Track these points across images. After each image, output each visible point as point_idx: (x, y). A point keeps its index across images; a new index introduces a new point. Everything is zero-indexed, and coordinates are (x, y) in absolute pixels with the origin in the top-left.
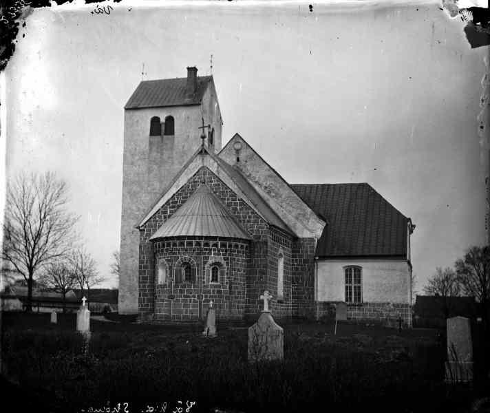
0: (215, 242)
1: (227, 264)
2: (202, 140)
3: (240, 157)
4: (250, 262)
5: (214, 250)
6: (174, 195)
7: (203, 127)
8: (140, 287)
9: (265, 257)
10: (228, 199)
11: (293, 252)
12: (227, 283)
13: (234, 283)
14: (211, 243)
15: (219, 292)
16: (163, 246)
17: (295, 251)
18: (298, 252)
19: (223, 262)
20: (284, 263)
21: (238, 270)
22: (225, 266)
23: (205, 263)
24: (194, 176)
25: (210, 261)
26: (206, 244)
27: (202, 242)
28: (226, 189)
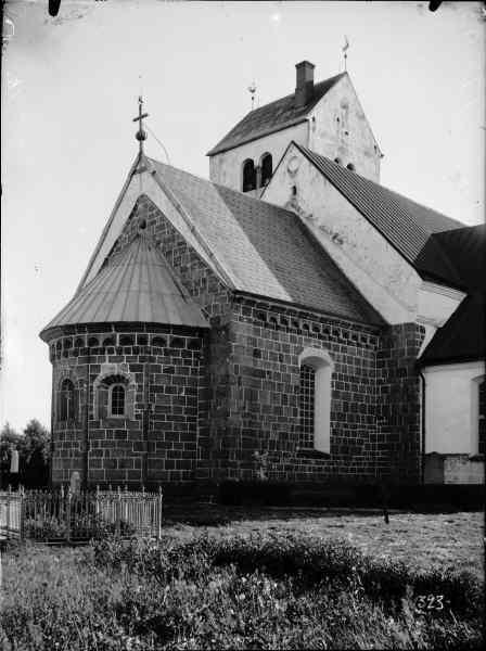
0: (108, 335)
1: (138, 378)
2: (138, 142)
5: (111, 351)
14: (102, 336)
19: (129, 374)
20: (334, 376)
21: (169, 390)
23: (94, 377)
25: (102, 375)
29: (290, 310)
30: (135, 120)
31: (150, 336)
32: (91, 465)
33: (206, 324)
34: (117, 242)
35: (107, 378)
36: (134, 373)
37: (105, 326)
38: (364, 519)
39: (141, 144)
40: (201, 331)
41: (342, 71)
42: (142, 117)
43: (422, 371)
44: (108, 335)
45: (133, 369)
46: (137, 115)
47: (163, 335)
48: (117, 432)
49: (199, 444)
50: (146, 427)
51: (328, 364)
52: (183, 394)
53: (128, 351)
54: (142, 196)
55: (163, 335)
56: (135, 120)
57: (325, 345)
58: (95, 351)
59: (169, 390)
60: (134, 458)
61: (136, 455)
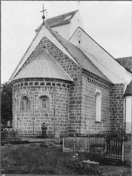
0: (42, 82)
1: (52, 97)
2: (43, 19)
3: (89, 53)
4: (71, 96)
5: (43, 87)
6: (29, 58)
7: (43, 11)
8: (81, 106)
9: (80, 91)
10: (58, 56)
11: (111, 93)
12: (52, 109)
13: (57, 109)
14: (40, 82)
15: (46, 115)
16: (22, 84)
17: (111, 94)
18: (114, 92)
19: (49, 96)
20: (102, 98)
21: (61, 101)
22: (50, 98)
23: (36, 96)
24: (39, 44)
25: (39, 95)
26: (36, 84)
27: (34, 82)
28: (57, 50)
29: (92, 76)
30: (41, 12)
31: (56, 83)
32: (36, 125)
33: (72, 80)
34: (33, 52)
35: (42, 96)
36: (51, 95)
37: (41, 79)
38: (42, 139)
39: (44, 20)
40: (70, 82)
41: (77, 9)
42: (43, 11)
43: (126, 97)
44: (42, 82)
45: (50, 93)
46: (42, 10)
47: (60, 83)
48: (45, 114)
49: (69, 119)
50: (54, 113)
51: (100, 94)
52: (65, 102)
53: (48, 88)
54: (44, 38)
55: (60, 83)
56: (41, 12)
57: (100, 89)
58: (37, 87)
59: (61, 101)
60: (51, 123)
61: (51, 122)
